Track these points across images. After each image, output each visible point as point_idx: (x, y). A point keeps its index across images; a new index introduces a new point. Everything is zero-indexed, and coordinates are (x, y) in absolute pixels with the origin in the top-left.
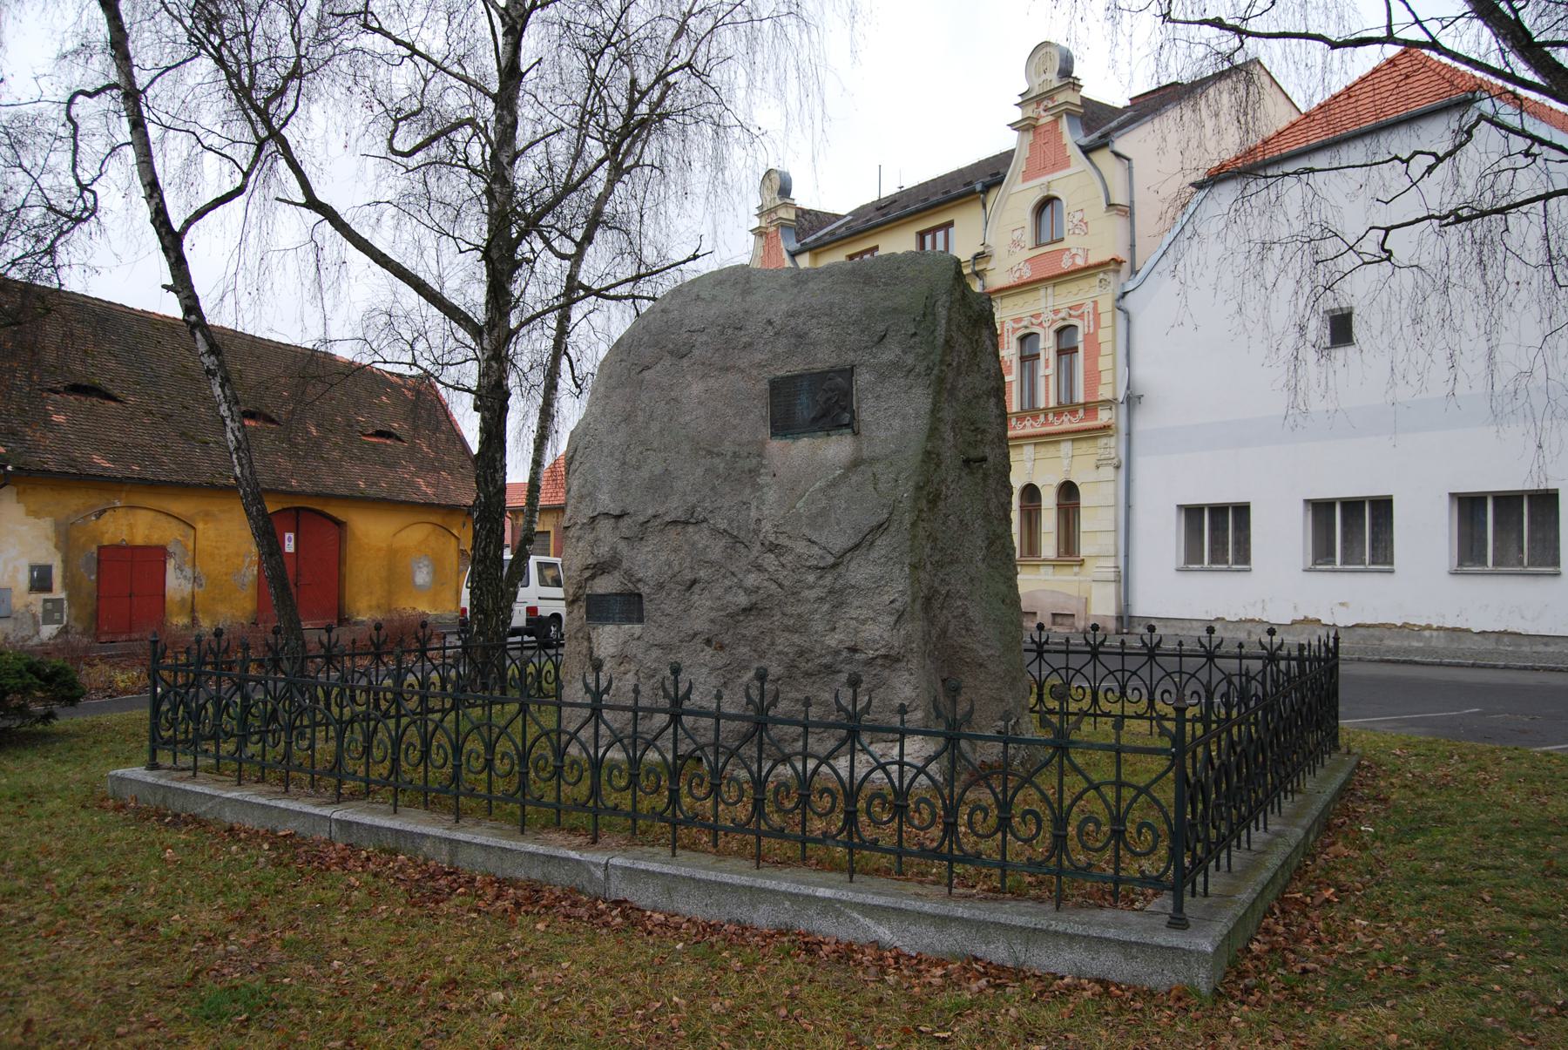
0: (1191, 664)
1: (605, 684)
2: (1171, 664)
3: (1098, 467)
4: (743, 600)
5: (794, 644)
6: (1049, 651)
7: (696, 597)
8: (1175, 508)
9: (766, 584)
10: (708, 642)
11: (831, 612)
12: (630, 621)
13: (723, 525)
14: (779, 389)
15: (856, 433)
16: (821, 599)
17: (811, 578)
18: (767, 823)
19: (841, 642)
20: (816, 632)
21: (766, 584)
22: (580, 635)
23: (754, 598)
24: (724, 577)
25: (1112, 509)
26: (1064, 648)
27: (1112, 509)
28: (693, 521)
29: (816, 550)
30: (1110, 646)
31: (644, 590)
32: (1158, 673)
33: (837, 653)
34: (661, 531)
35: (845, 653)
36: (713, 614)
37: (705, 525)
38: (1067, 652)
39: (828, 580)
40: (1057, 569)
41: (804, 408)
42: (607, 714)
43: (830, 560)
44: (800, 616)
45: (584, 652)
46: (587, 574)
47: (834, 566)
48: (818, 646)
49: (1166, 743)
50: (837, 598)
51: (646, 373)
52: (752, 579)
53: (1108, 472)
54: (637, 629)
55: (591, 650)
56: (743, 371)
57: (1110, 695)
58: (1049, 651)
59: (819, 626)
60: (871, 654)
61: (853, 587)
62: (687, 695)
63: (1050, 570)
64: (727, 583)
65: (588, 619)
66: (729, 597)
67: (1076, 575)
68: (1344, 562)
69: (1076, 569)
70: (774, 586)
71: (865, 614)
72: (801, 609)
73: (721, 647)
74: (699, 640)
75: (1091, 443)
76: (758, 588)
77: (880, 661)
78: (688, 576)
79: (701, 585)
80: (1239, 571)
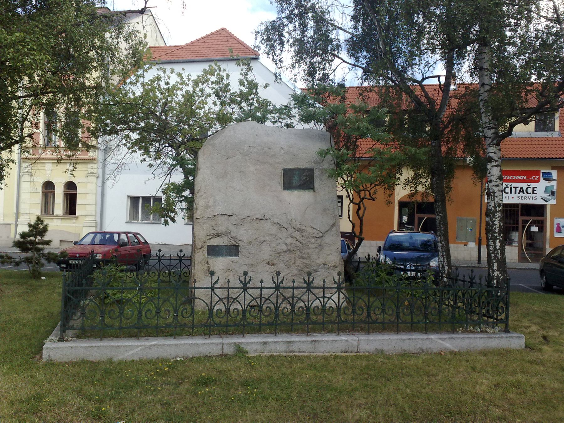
0: (174, 263)
1: (312, 280)
2: (166, 263)
3: (87, 177)
4: (285, 248)
5: (304, 263)
6: (183, 260)
7: (264, 246)
8: (126, 197)
9: (295, 242)
10: (268, 263)
11: (319, 252)
12: (231, 255)
13: (276, 221)
14: (287, 172)
15: (314, 191)
16: (316, 248)
17: (313, 241)
18: (372, 319)
19: (321, 262)
20: (314, 259)
21: (295, 242)
22: (204, 261)
23: (289, 247)
24: (277, 240)
25: (94, 195)
26: (169, 258)
27: (94, 195)
28: (264, 219)
29: (315, 231)
30: (186, 257)
31: (240, 243)
32: (183, 266)
33: (319, 265)
34: (250, 222)
35: (322, 266)
36: (271, 253)
37: (269, 220)
38: (170, 260)
39: (319, 241)
40: (63, 220)
41: (296, 181)
42: (217, 291)
43: (321, 235)
44: (308, 253)
45: (206, 268)
46: (209, 237)
47: (321, 237)
48: (313, 263)
49: (281, 290)
50: (320, 247)
51: (229, 160)
52: (289, 241)
53: (93, 179)
54: (235, 259)
55: (209, 268)
56: (271, 165)
57: (185, 274)
58: (183, 260)
59: (314, 256)
60: (330, 265)
61: (326, 243)
62: (282, 282)
63: (59, 221)
64: (278, 242)
65: (208, 254)
66: (279, 247)
67: (74, 223)
68: (153, 220)
69: (74, 221)
70: (298, 243)
71: (329, 252)
72: (309, 251)
73: (273, 265)
74: (265, 262)
75: (84, 165)
76: (292, 244)
77: (332, 268)
78: (262, 239)
79: (267, 242)
80: (156, 223)
